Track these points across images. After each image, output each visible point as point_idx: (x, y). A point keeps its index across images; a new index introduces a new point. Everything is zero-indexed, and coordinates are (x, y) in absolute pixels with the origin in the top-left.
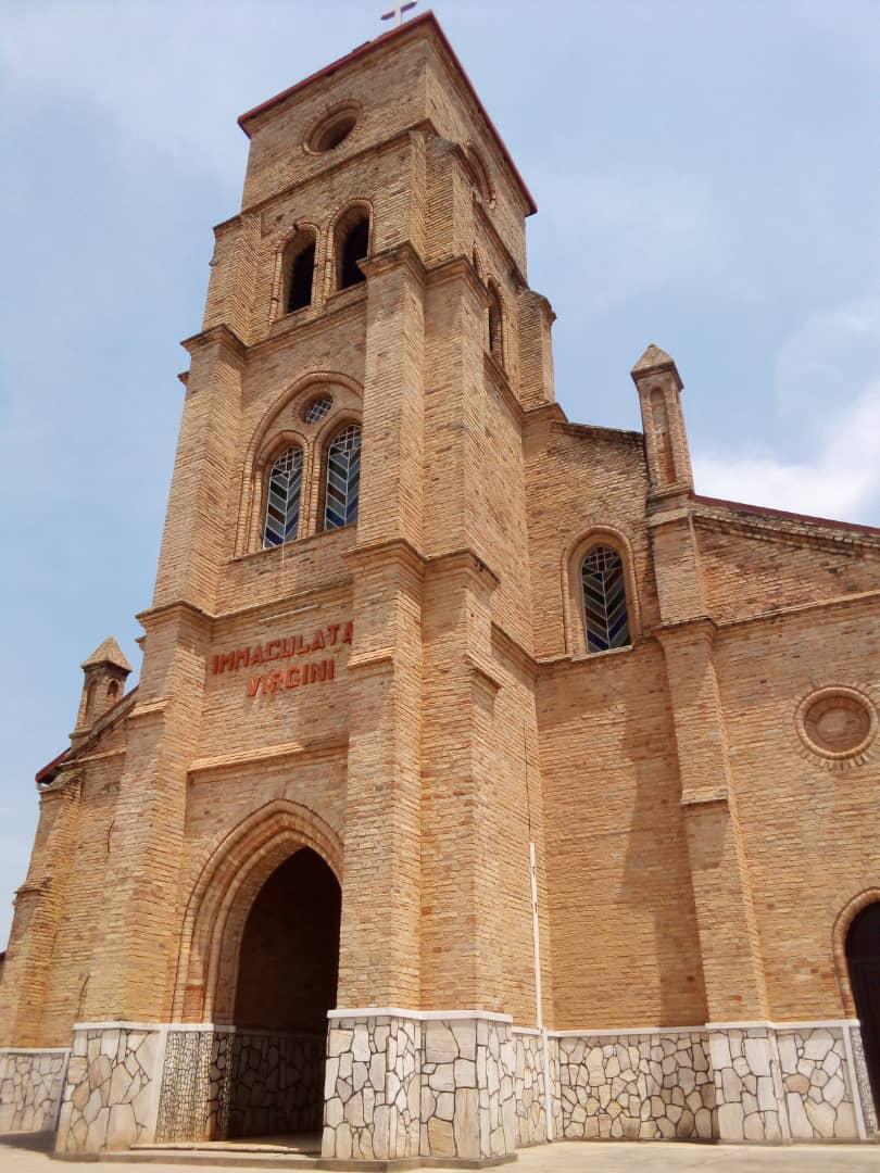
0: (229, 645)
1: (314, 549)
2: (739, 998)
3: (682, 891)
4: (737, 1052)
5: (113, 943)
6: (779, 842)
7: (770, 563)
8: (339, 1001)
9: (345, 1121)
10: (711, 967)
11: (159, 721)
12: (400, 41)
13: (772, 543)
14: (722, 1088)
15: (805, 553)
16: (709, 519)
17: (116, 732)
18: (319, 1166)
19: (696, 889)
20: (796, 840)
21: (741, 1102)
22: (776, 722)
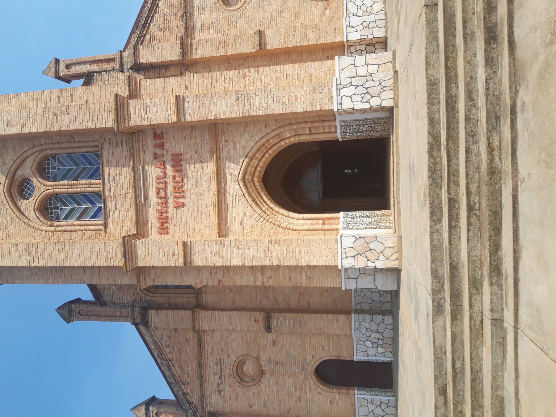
1: (109, 174)
2: (335, 29)
3: (294, 60)
4: (354, 29)
5: (300, 253)
6: (278, 19)
7: (162, 18)
8: (330, 108)
9: (378, 96)
10: (323, 41)
11: (189, 243)
13: (153, 16)
14: (367, 35)
16: (136, 41)
17: (189, 391)
18: (397, 106)
19: (293, 46)
20: (277, 13)
21: (372, 28)
22: (230, 19)
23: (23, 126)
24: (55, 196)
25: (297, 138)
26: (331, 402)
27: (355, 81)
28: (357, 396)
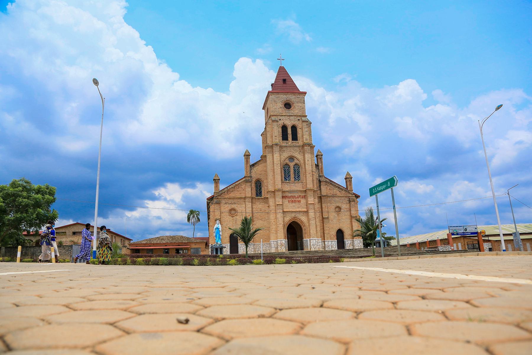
5: (281, 231)
12: (301, 94)
24: (290, 167)
28: (228, 244)
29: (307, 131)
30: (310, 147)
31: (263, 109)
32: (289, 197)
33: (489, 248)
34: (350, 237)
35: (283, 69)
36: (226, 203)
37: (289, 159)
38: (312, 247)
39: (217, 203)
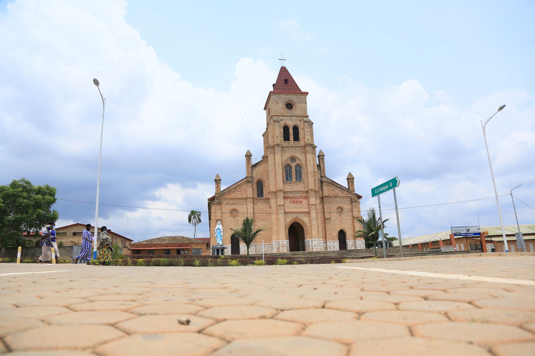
0: (286, 195)
4: (330, 243)
12: (302, 94)
15: (339, 189)
23: (309, 165)
24: (291, 168)
25: (306, 230)
26: (227, 237)
27: (318, 243)
29: (309, 132)
30: (311, 148)
31: (264, 109)
32: (291, 198)
33: (492, 249)
34: (352, 237)
35: (285, 69)
36: (227, 204)
37: (291, 159)
38: (314, 247)
39: (218, 204)
